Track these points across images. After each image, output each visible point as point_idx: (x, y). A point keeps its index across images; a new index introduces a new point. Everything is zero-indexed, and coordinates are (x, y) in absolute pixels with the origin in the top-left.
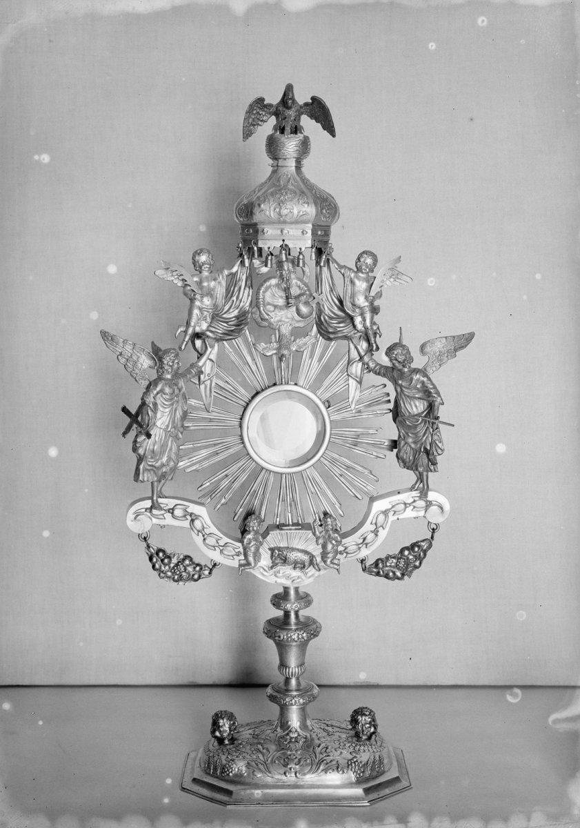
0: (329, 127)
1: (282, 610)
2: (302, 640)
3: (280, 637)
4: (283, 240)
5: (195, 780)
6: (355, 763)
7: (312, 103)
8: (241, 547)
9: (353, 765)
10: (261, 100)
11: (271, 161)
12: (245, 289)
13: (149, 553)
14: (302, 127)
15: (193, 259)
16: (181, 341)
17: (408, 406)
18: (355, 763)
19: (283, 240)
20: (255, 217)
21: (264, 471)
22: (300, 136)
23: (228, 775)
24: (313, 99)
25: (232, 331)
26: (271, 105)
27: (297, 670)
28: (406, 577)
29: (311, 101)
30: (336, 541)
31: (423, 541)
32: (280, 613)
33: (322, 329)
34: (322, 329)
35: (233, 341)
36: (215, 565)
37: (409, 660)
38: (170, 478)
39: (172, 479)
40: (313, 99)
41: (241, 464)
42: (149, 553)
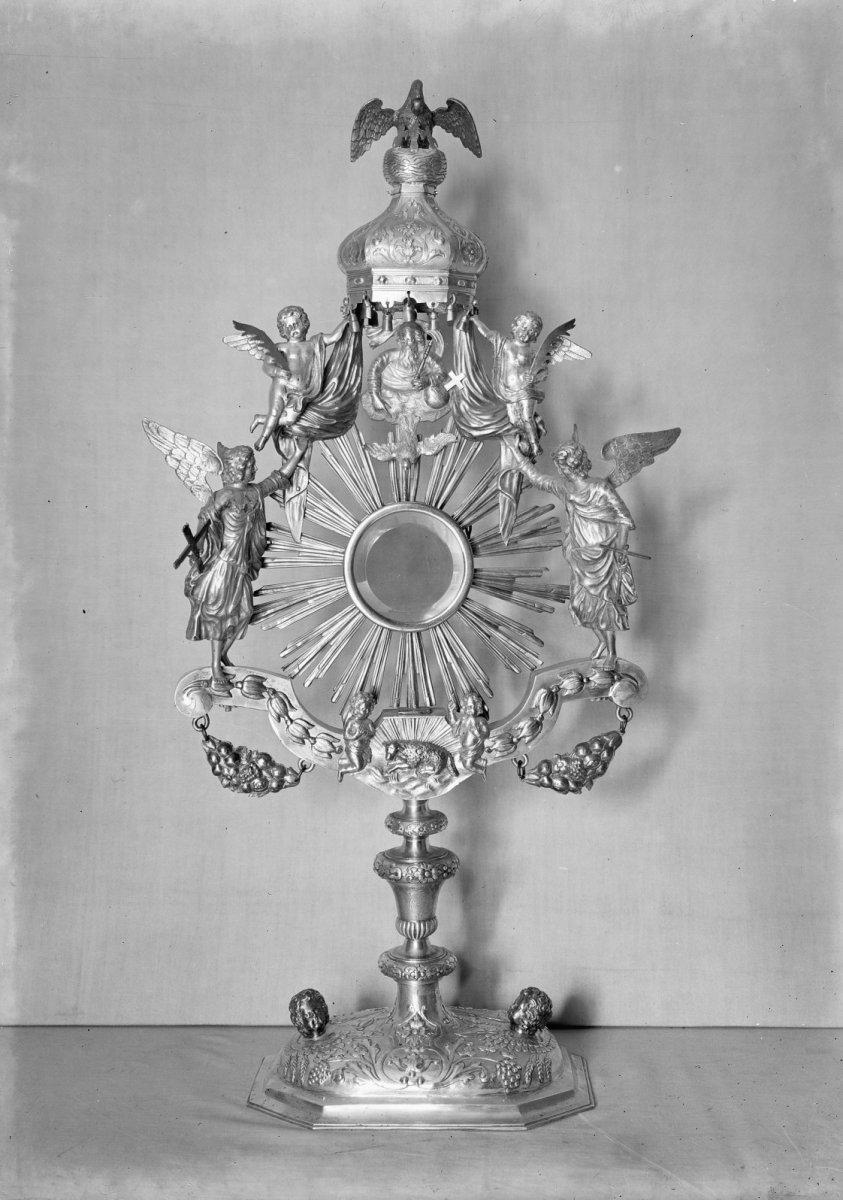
0: (473, 144)
1: (400, 834)
2: (430, 880)
3: (396, 874)
4: (409, 292)
5: (268, 1091)
6: (505, 1066)
7: (448, 110)
8: (343, 740)
9: (503, 1069)
10: (377, 103)
11: (391, 188)
12: (351, 366)
13: (207, 749)
14: (434, 140)
15: (280, 317)
16: (259, 437)
17: (584, 532)
18: (505, 1066)
19: (409, 292)
20: (367, 258)
21: (379, 505)
22: (430, 151)
23: (318, 1082)
24: (450, 103)
25: (333, 425)
26: (391, 112)
27: (417, 926)
28: (584, 789)
29: (446, 106)
30: (436, 427)
31: (608, 735)
32: (398, 842)
33: (461, 423)
34: (461, 423)
35: (338, 439)
36: (304, 769)
37: (625, 1114)
38: (239, 636)
39: (241, 638)
40: (450, 103)
41: (343, 516)
42: (207, 749)
